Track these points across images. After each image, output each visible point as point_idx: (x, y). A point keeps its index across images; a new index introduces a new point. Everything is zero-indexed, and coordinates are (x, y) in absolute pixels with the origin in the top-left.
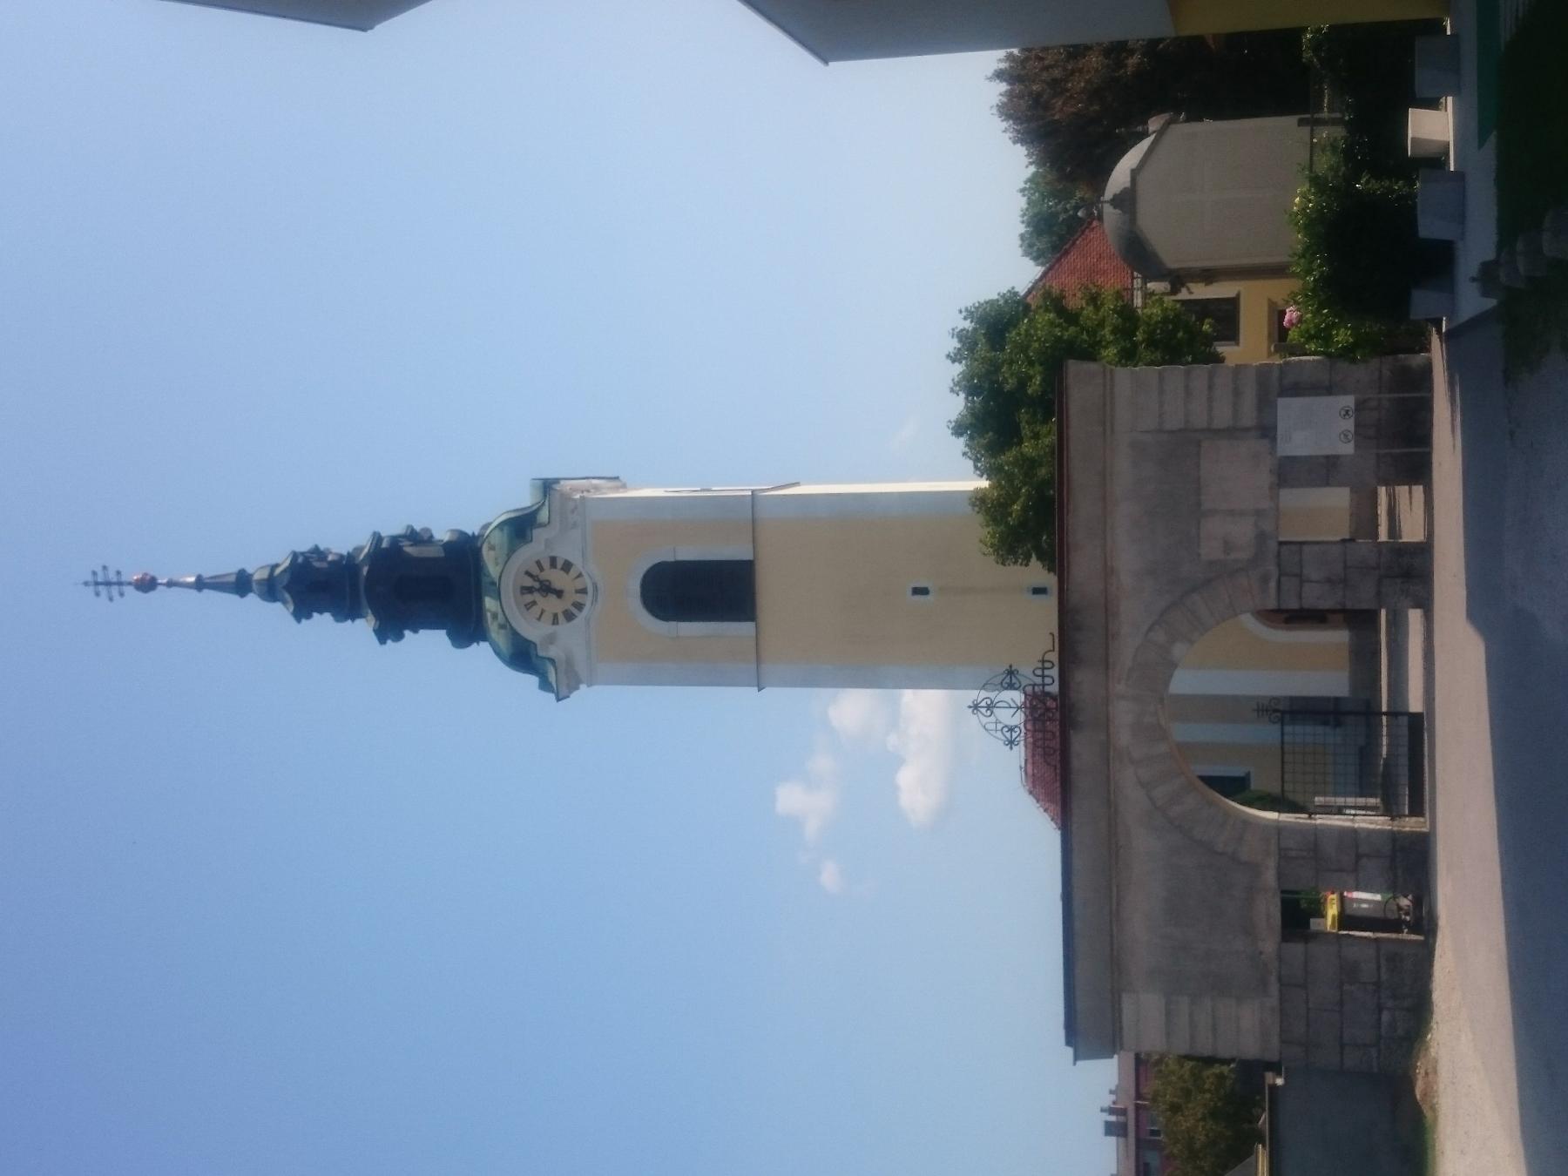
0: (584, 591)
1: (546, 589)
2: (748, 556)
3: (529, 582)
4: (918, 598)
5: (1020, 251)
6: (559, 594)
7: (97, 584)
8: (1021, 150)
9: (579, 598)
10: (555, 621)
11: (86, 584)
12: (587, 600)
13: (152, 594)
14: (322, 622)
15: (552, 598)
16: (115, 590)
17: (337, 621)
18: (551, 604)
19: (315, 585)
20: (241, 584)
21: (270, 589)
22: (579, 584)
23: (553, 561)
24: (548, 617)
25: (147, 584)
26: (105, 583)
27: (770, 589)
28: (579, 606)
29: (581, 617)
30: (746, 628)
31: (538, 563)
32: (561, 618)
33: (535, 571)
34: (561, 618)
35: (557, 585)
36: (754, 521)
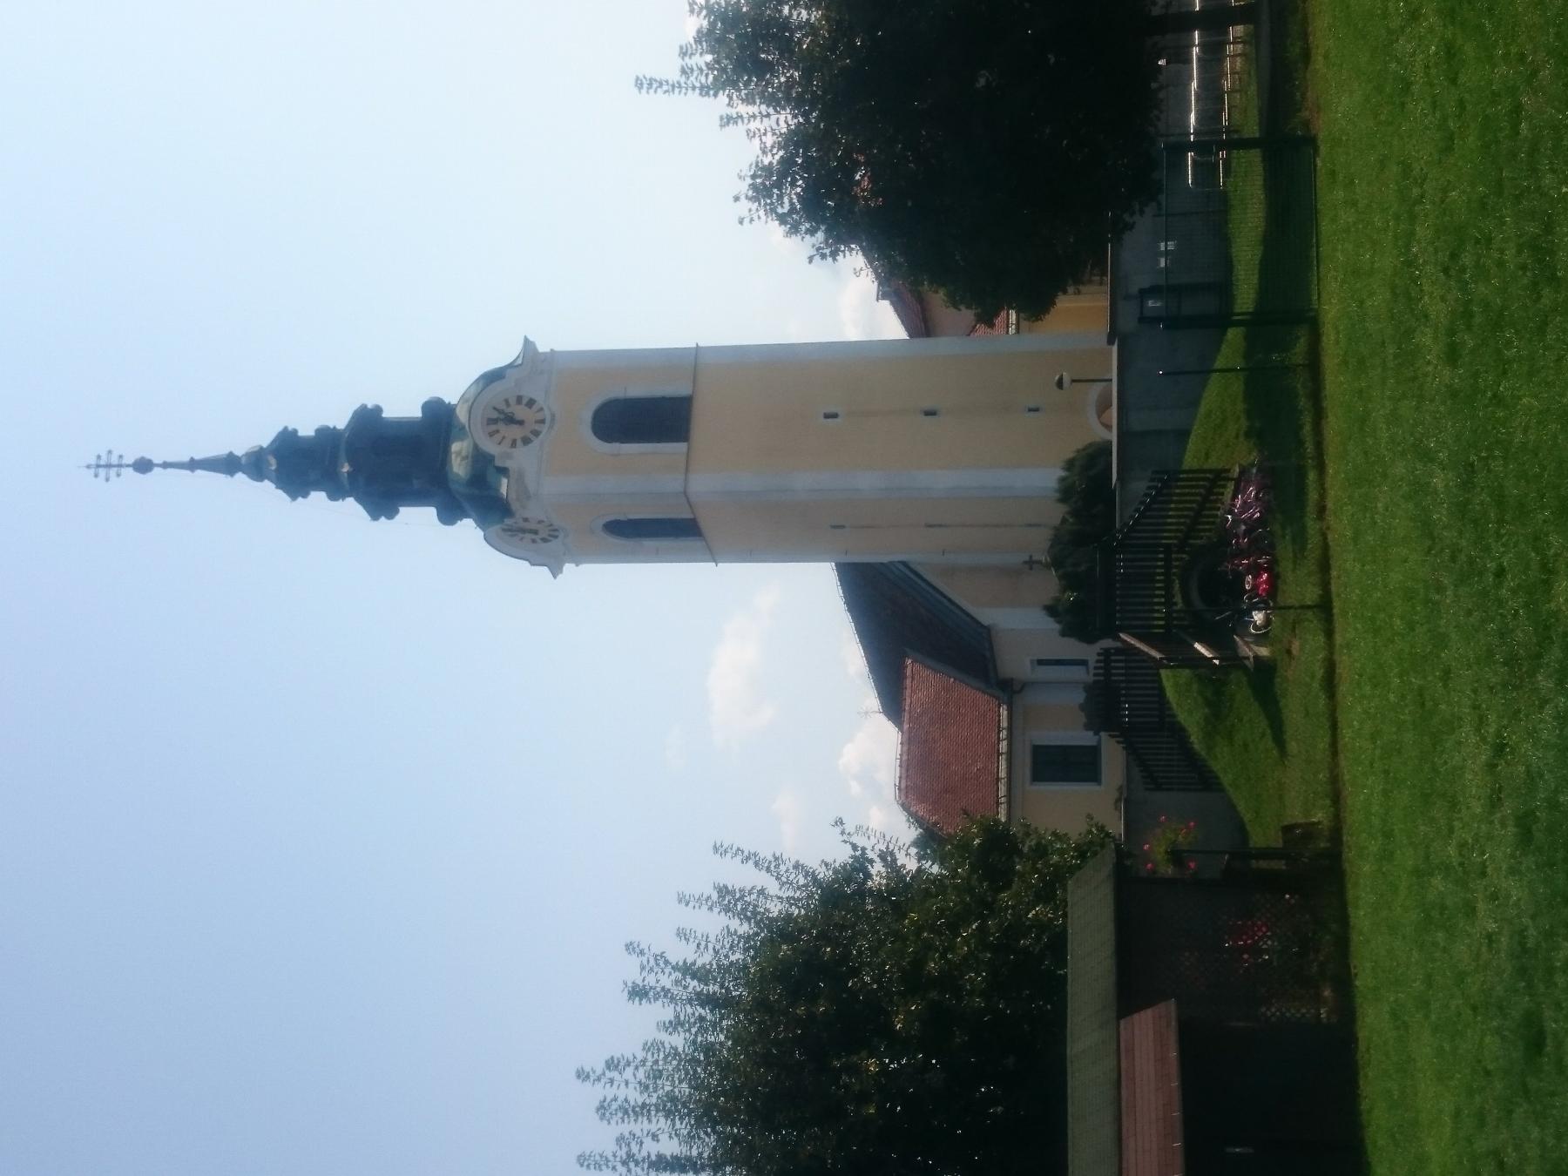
0: (542, 421)
1: (511, 420)
3: (495, 415)
4: (833, 410)
7: (98, 466)
8: (547, 350)
9: (537, 427)
10: (514, 444)
11: (88, 467)
12: (544, 429)
13: (148, 475)
15: (515, 427)
16: (113, 472)
17: (294, 497)
18: (515, 432)
19: (300, 464)
20: (228, 465)
21: (254, 465)
22: (539, 416)
23: (519, 400)
24: (508, 442)
25: (143, 466)
26: (105, 466)
28: (536, 433)
29: (536, 442)
30: (681, 447)
31: (507, 401)
32: (519, 443)
33: (503, 407)
34: (519, 443)
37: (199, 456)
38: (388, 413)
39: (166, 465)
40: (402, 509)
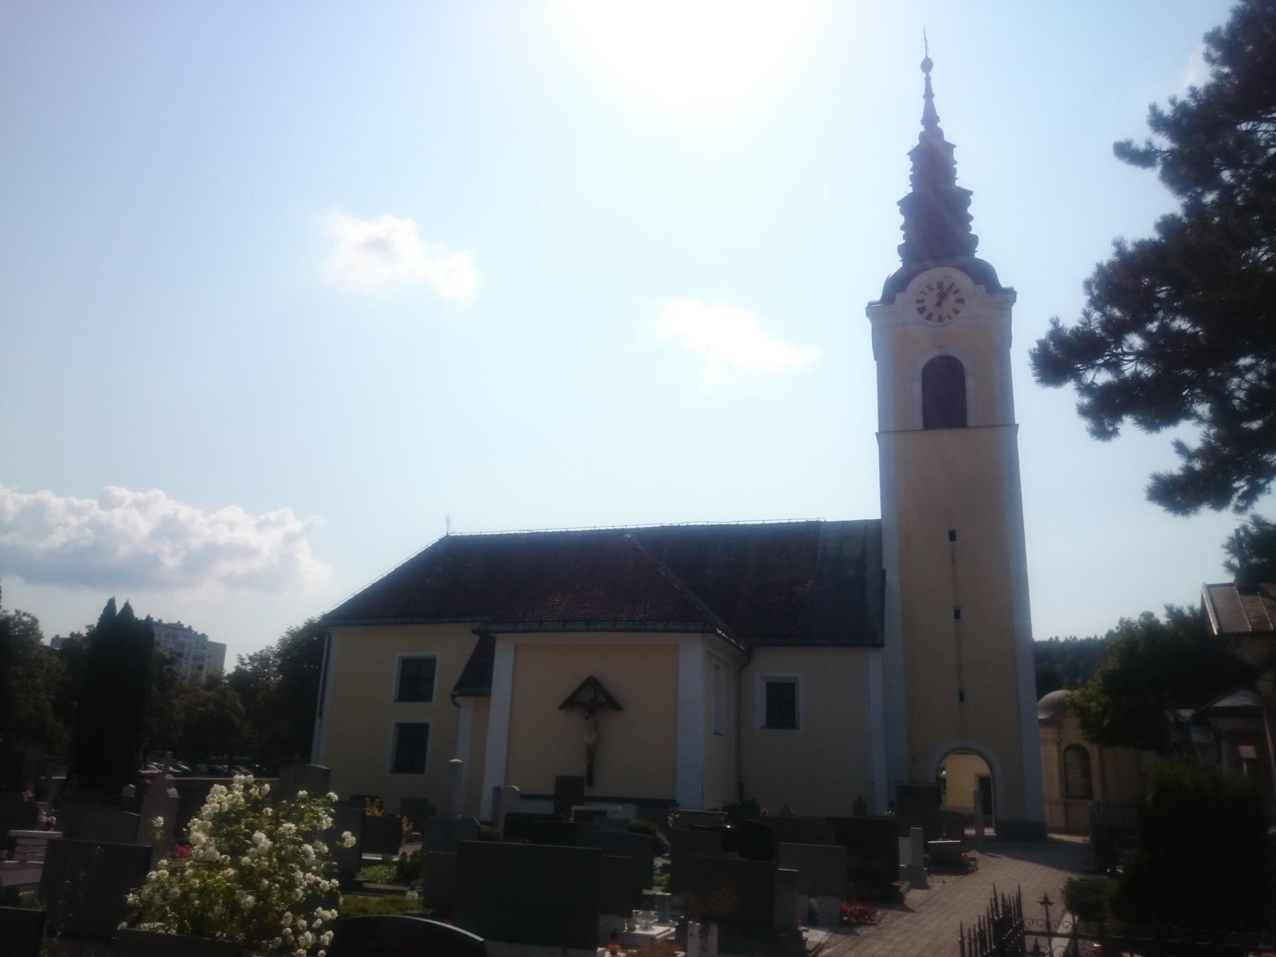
1: (942, 296)
2: (971, 421)
5: (1089, 271)
6: (939, 304)
14: (1004, 281)
15: (936, 300)
18: (932, 299)
19: (933, 162)
23: (961, 301)
27: (946, 437)
30: (919, 422)
35: (944, 303)
36: (993, 426)
37: (936, 101)
38: (210, 639)
39: (928, 80)
40: (910, 190)
